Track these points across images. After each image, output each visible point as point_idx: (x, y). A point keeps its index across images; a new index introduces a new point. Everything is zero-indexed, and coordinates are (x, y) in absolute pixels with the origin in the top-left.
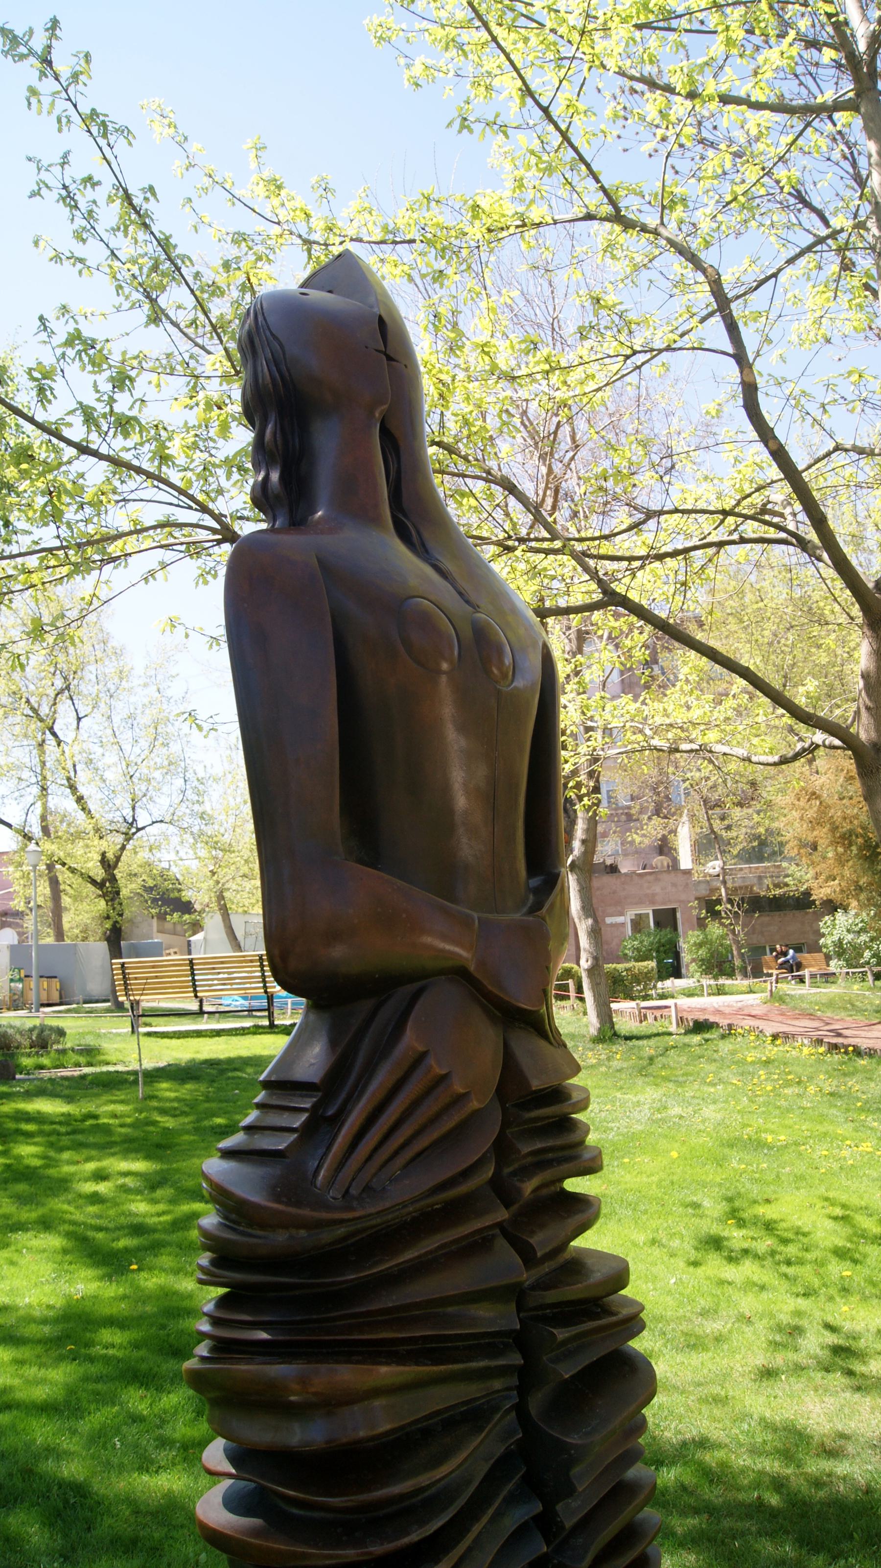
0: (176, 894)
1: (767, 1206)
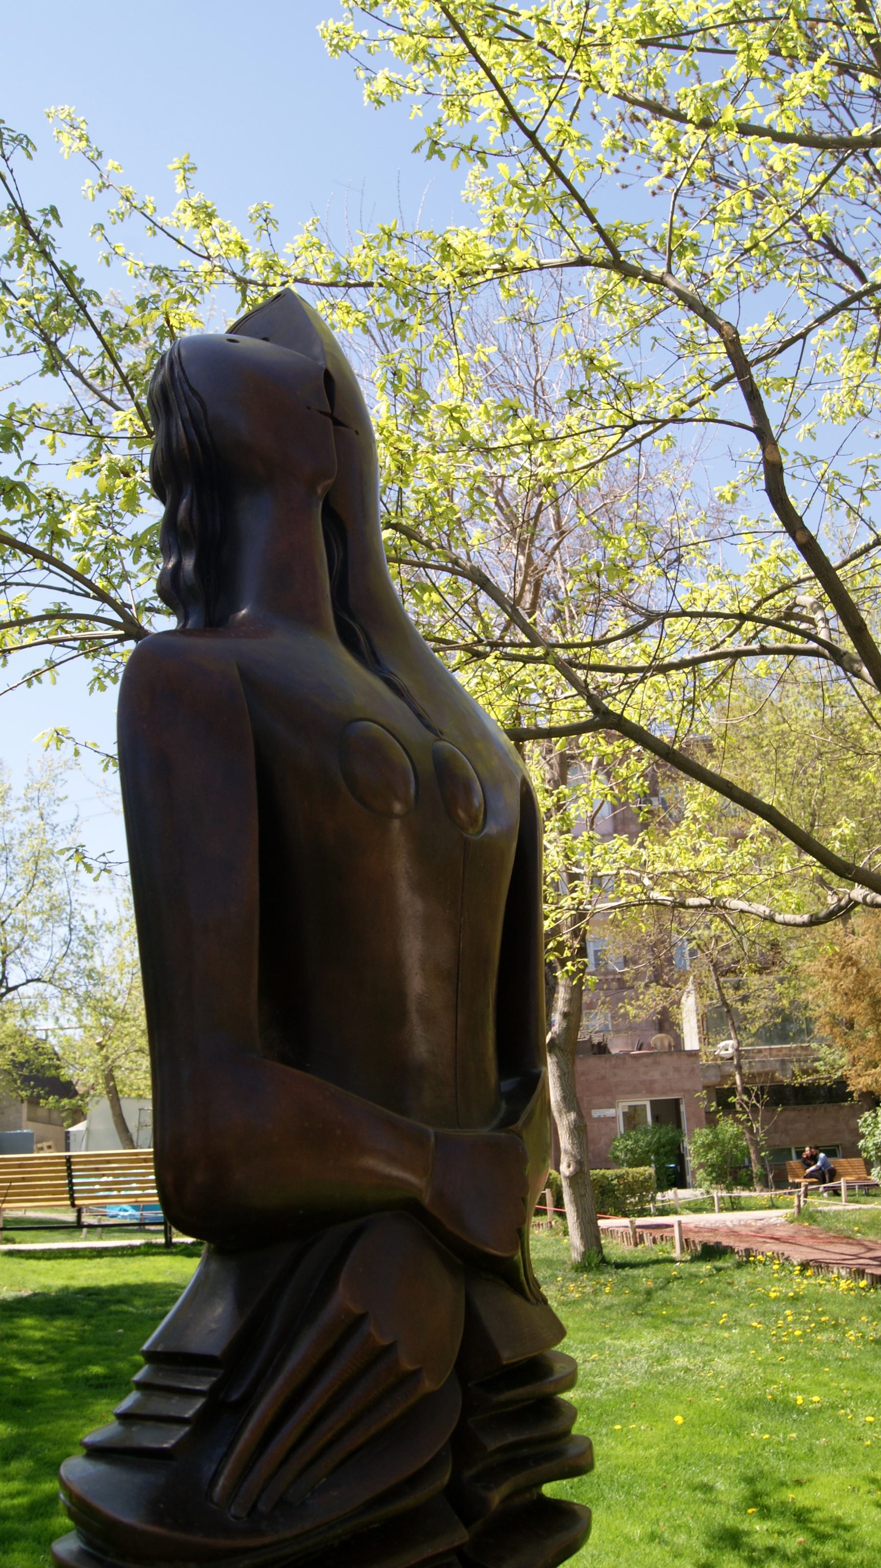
0: (53, 1072)
1: (798, 1490)
